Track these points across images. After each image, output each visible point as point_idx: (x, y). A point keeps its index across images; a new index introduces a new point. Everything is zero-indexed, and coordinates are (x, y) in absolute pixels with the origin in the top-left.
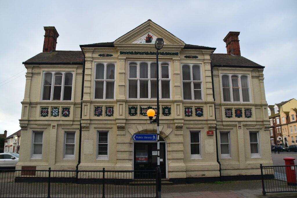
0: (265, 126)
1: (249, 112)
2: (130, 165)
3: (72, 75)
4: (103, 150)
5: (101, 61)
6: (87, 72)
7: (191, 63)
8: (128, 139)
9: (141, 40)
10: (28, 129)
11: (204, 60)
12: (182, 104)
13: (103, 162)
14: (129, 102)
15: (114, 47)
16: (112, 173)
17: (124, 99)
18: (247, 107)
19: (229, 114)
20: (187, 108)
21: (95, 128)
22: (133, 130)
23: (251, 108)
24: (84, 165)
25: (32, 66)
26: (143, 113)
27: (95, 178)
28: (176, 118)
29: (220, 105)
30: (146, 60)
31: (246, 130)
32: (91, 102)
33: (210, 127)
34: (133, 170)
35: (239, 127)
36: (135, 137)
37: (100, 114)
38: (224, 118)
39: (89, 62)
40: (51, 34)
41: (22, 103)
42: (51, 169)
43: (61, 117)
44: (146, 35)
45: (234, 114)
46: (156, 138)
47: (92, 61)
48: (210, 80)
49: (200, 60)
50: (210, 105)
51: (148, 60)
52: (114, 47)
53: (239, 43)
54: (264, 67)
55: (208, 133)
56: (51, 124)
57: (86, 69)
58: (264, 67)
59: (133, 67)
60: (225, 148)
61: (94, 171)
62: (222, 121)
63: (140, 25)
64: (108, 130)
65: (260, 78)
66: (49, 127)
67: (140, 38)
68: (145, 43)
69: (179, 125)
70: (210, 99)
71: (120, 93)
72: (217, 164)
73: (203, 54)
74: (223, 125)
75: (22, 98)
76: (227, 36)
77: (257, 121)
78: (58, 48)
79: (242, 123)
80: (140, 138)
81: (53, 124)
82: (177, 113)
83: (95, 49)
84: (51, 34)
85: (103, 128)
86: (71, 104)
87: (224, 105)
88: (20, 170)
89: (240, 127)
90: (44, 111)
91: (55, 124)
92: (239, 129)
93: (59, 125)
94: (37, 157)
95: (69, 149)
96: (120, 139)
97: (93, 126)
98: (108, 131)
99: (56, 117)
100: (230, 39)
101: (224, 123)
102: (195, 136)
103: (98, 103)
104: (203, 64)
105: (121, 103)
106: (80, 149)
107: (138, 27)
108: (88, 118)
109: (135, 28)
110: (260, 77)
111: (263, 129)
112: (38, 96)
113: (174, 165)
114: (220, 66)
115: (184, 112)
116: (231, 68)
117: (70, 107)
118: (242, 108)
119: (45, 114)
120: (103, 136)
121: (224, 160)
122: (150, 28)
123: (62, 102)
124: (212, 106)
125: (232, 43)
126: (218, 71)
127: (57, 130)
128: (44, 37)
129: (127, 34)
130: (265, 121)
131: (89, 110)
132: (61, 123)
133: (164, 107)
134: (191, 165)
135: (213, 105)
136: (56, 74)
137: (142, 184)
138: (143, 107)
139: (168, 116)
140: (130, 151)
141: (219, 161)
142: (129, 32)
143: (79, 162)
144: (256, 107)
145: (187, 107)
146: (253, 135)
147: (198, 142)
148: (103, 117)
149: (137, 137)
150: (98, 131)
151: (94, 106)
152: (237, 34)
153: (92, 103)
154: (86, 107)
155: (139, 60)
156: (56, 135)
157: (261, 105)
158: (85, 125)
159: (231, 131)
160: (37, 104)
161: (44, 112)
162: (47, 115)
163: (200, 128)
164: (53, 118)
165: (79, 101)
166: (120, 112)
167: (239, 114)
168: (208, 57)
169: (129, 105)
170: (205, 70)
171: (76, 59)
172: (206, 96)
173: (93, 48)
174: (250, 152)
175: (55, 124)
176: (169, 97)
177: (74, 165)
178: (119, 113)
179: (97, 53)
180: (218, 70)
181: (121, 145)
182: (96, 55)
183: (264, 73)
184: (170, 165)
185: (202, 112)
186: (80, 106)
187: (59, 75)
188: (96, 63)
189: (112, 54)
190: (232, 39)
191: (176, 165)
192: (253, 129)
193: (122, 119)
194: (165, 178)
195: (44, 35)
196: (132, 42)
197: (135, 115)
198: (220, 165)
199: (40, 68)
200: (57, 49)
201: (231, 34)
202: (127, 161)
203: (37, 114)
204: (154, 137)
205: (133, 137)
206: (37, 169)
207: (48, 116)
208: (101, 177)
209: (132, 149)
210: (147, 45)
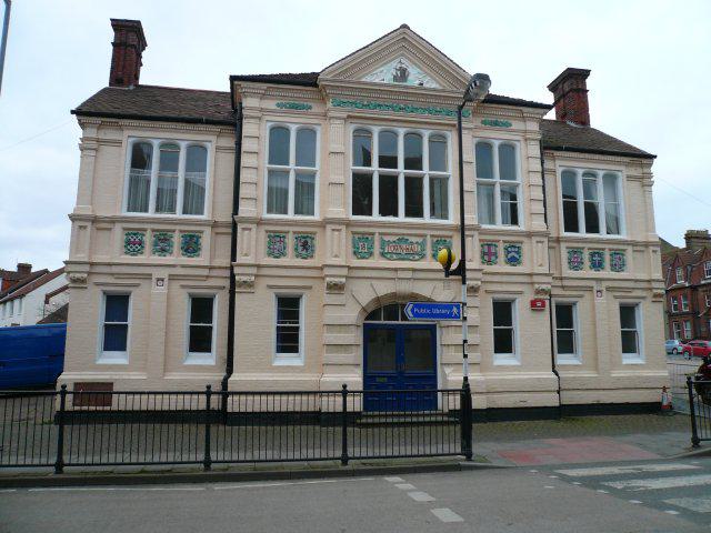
0: (655, 291)
2: (355, 379)
3: (205, 149)
6: (246, 145)
7: (496, 137)
8: (352, 314)
9: (383, 75)
10: (89, 285)
11: (525, 132)
13: (289, 371)
14: (353, 226)
15: (316, 85)
16: (311, 398)
18: (615, 247)
21: (270, 287)
22: (366, 293)
24: (238, 379)
25: (99, 120)
27: (271, 409)
28: (536, 272)
29: (558, 240)
32: (260, 222)
33: (538, 292)
34: (361, 389)
37: (282, 254)
39: (252, 121)
40: (129, 39)
41: (73, 218)
42: (212, 390)
44: (395, 64)
45: (377, 250)
48: (537, 179)
50: (538, 239)
51: (400, 124)
52: (316, 85)
54: (655, 157)
55: (533, 304)
58: (655, 157)
59: (362, 136)
60: (565, 343)
61: (267, 393)
64: (511, 296)
65: (645, 181)
66: (147, 281)
68: (392, 82)
69: (337, 280)
71: (333, 202)
73: (524, 119)
75: (70, 204)
77: (211, 268)
78: (146, 78)
81: (157, 273)
84: (129, 39)
85: (289, 285)
88: (202, 393)
91: (164, 273)
94: (116, 358)
95: (200, 341)
96: (333, 315)
98: (514, 300)
101: (566, 283)
103: (277, 225)
105: (338, 227)
111: (650, 299)
112: (115, 204)
114: (559, 149)
116: (582, 155)
117: (202, 232)
118: (603, 249)
120: (288, 307)
121: (564, 367)
126: (554, 160)
128: (112, 47)
130: (654, 280)
133: (435, 240)
135: (546, 240)
136: (584, 175)
137: (412, 424)
138: (386, 238)
141: (556, 369)
143: (230, 371)
144: (635, 248)
146: (627, 314)
147: (571, 326)
150: (190, 295)
151: (267, 231)
152: (585, 74)
155: (377, 123)
159: (641, 305)
160: (113, 221)
161: (133, 243)
162: (284, 254)
163: (515, 293)
165: (225, 216)
166: (333, 250)
167: (162, 243)
168: (534, 126)
169: (354, 233)
170: (528, 155)
171: (221, 112)
173: (265, 86)
174: (620, 349)
175: (164, 273)
176: (447, 218)
177: (215, 379)
180: (554, 158)
181: (335, 325)
182: (271, 104)
183: (653, 169)
189: (309, 104)
190: (571, 86)
194: (436, 409)
196: (364, 76)
199: (121, 128)
200: (142, 81)
202: (352, 368)
203: (111, 249)
204: (455, 310)
206: (115, 389)
207: (142, 253)
208: (203, 406)
210: (399, 86)
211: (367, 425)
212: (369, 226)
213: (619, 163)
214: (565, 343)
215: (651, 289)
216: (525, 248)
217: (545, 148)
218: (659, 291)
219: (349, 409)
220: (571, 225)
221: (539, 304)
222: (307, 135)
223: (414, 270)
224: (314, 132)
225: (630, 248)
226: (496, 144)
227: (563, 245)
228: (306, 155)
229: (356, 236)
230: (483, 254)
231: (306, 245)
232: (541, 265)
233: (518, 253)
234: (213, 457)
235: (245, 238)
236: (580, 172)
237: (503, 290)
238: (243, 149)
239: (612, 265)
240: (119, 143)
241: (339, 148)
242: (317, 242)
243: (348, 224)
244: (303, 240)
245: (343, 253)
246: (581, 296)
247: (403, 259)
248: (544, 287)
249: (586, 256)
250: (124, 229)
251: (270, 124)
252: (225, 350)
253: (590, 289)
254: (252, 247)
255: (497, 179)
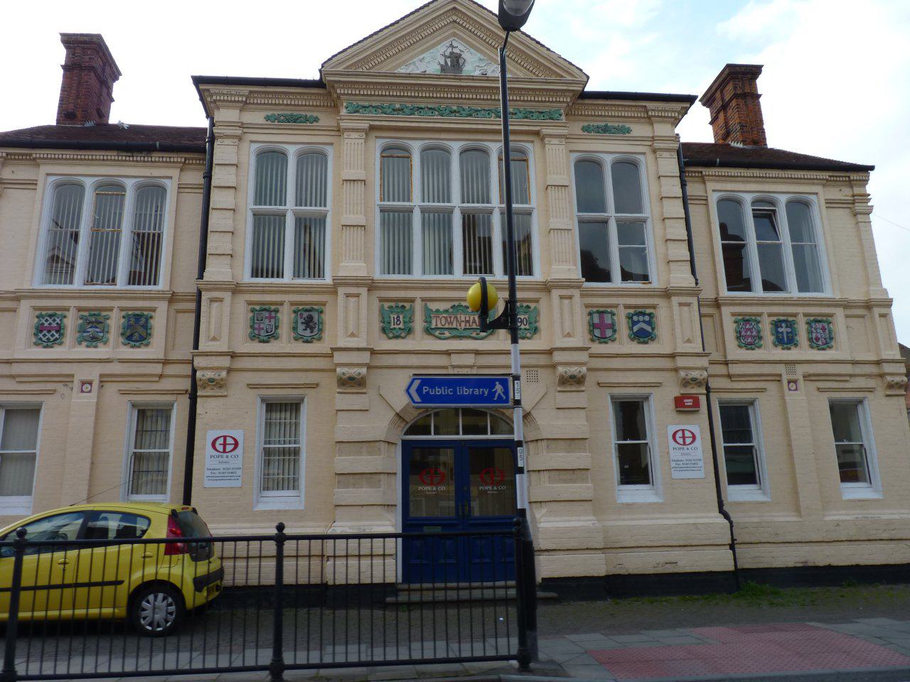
0: (889, 378)
1: (824, 329)
4: (280, 465)
5: (276, 138)
6: (219, 177)
7: (608, 150)
9: (429, 62)
12: (582, 296)
17: (363, 273)
19: (748, 337)
20: (598, 312)
21: (252, 386)
23: (831, 315)
26: (437, 329)
28: (558, 345)
29: (717, 304)
30: (443, 136)
31: (817, 393)
32: (236, 289)
33: (686, 383)
35: (789, 382)
36: (419, 391)
37: (272, 336)
38: (735, 352)
39: (227, 141)
43: (116, 347)
44: (443, 48)
45: (419, 324)
46: (506, 392)
47: (240, 138)
49: (636, 139)
53: (759, 102)
54: (872, 168)
55: (679, 402)
56: (73, 376)
57: (217, 167)
58: (872, 168)
59: (395, 156)
60: (741, 466)
62: (726, 363)
63: (421, 8)
64: (295, 392)
65: (858, 207)
67: (421, 57)
70: (681, 277)
72: (726, 521)
73: (649, 120)
74: (729, 376)
76: (717, 84)
79: (801, 370)
80: (438, 391)
81: (82, 373)
82: (561, 324)
83: (251, 92)
85: (280, 381)
86: (158, 297)
87: (732, 302)
89: (795, 382)
90: (46, 324)
92: (790, 390)
93: (105, 379)
96: (349, 428)
97: (240, 380)
99: (95, 349)
100: (729, 91)
101: (734, 369)
102: (630, 415)
104: (650, 157)
106: (198, 343)
107: (412, 13)
108: (225, 349)
109: (403, 19)
110: (856, 204)
111: (881, 392)
113: (557, 525)
115: (586, 327)
117: (154, 310)
118: (795, 315)
119: (53, 335)
122: (455, 21)
123: (80, 291)
124: (688, 305)
125: (734, 103)
127: (98, 398)
128: (62, 71)
129: (371, 36)
131: (226, 320)
132: (117, 369)
134: (621, 524)
135: (694, 300)
136: (755, 202)
138: (433, 306)
139: (529, 338)
140: (388, 474)
141: (726, 508)
142: (381, 30)
144: (849, 312)
145: (595, 310)
148: (285, 343)
149: (425, 389)
151: (249, 303)
152: (755, 71)
153: (241, 292)
154: (215, 305)
156: (93, 418)
157: (869, 305)
158: (209, 374)
160: (17, 297)
161: (48, 330)
164: (83, 352)
166: (352, 325)
167: (93, 329)
169: (382, 300)
172: (667, 270)
175: (93, 373)
178: (346, 328)
179: (262, 110)
180: (703, 180)
182: (257, 117)
183: (869, 188)
184: (547, 526)
185: (653, 329)
186: (193, 306)
187: (110, 191)
188: (255, 147)
189: (315, 114)
190: (736, 89)
191: (567, 524)
192: (844, 390)
193: (358, 349)
195: (63, 63)
196: (399, 66)
197: (391, 335)
198: (731, 523)
199: (35, 162)
200: (113, 119)
201: (730, 74)
204: (499, 388)
205: (407, 391)
207: (61, 344)
209: (396, 464)
211: (410, 605)
212: (406, 288)
213: (746, 179)
214: (741, 466)
215: (882, 376)
216: (662, 315)
217: (687, 164)
218: (897, 379)
219: (288, 579)
220: (737, 279)
221: (689, 402)
222: (313, 159)
223: (477, 353)
224: (323, 156)
225: (839, 313)
226: (608, 160)
227: (726, 311)
228: (312, 189)
229: (386, 305)
230: (593, 326)
231: (310, 322)
232: (689, 341)
233: (649, 323)
234: (288, 658)
235: (214, 313)
236: (748, 198)
237: (629, 383)
238: (214, 183)
239: (810, 340)
240: (33, 184)
241: (358, 174)
242: (327, 317)
243: (372, 286)
244: (305, 315)
245: (363, 329)
246: (762, 390)
247: (460, 337)
248: (695, 374)
249: (766, 327)
250: (35, 308)
251: (255, 147)
252: (182, 489)
253: (777, 378)
254: (225, 325)
255: (611, 212)
